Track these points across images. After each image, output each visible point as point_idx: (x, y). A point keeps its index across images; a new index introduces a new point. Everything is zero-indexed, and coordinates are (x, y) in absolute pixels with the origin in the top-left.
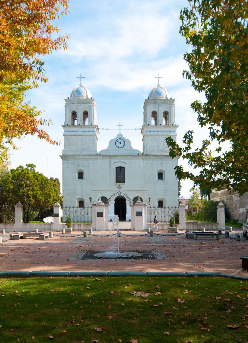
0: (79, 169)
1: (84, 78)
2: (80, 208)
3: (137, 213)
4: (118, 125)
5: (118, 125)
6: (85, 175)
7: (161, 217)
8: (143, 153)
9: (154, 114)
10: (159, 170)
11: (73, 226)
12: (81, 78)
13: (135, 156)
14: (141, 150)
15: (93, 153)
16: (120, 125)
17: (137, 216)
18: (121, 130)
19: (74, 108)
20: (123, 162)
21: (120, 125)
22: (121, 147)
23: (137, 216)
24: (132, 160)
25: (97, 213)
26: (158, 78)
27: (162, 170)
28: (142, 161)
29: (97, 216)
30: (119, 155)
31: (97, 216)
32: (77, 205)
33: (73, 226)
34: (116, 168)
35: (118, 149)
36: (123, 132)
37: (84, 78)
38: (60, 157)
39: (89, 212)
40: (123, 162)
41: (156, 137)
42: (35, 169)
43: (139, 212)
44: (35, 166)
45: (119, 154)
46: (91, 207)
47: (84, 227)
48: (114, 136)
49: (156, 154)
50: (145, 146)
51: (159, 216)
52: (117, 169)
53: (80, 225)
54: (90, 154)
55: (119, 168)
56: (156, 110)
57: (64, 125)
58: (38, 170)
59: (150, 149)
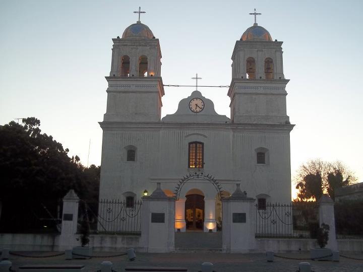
0: (130, 144)
1: (144, 12)
2: (128, 209)
3: (234, 215)
4: (193, 78)
5: (193, 78)
6: (139, 154)
7: (284, 224)
8: (233, 121)
9: (251, 62)
10: (259, 148)
11: (102, 240)
12: (140, 12)
13: (221, 124)
14: (229, 116)
15: (152, 120)
16: (197, 78)
17: (234, 221)
18: (196, 85)
19: (126, 51)
20: (201, 135)
21: (197, 78)
22: (201, 101)
23: (234, 221)
24: (216, 132)
25: (153, 214)
26: (255, 14)
27: (263, 148)
28: (231, 133)
29: (153, 221)
30: (195, 123)
31: (153, 221)
32: (123, 199)
33: (102, 240)
34: (190, 144)
35: (193, 113)
36: (199, 89)
37: (144, 12)
38: (100, 126)
39: (137, 211)
40: (201, 135)
41: (254, 97)
42: (40, 128)
43: (240, 214)
44: (38, 122)
45: (195, 122)
46: (140, 202)
47: (124, 244)
48: (187, 93)
49: (254, 123)
50: (236, 110)
51: (281, 222)
52: (191, 145)
53: (116, 239)
54: (148, 121)
55: (194, 145)
56: (254, 56)
57: (109, 75)
58: (45, 129)
59: (244, 115)
